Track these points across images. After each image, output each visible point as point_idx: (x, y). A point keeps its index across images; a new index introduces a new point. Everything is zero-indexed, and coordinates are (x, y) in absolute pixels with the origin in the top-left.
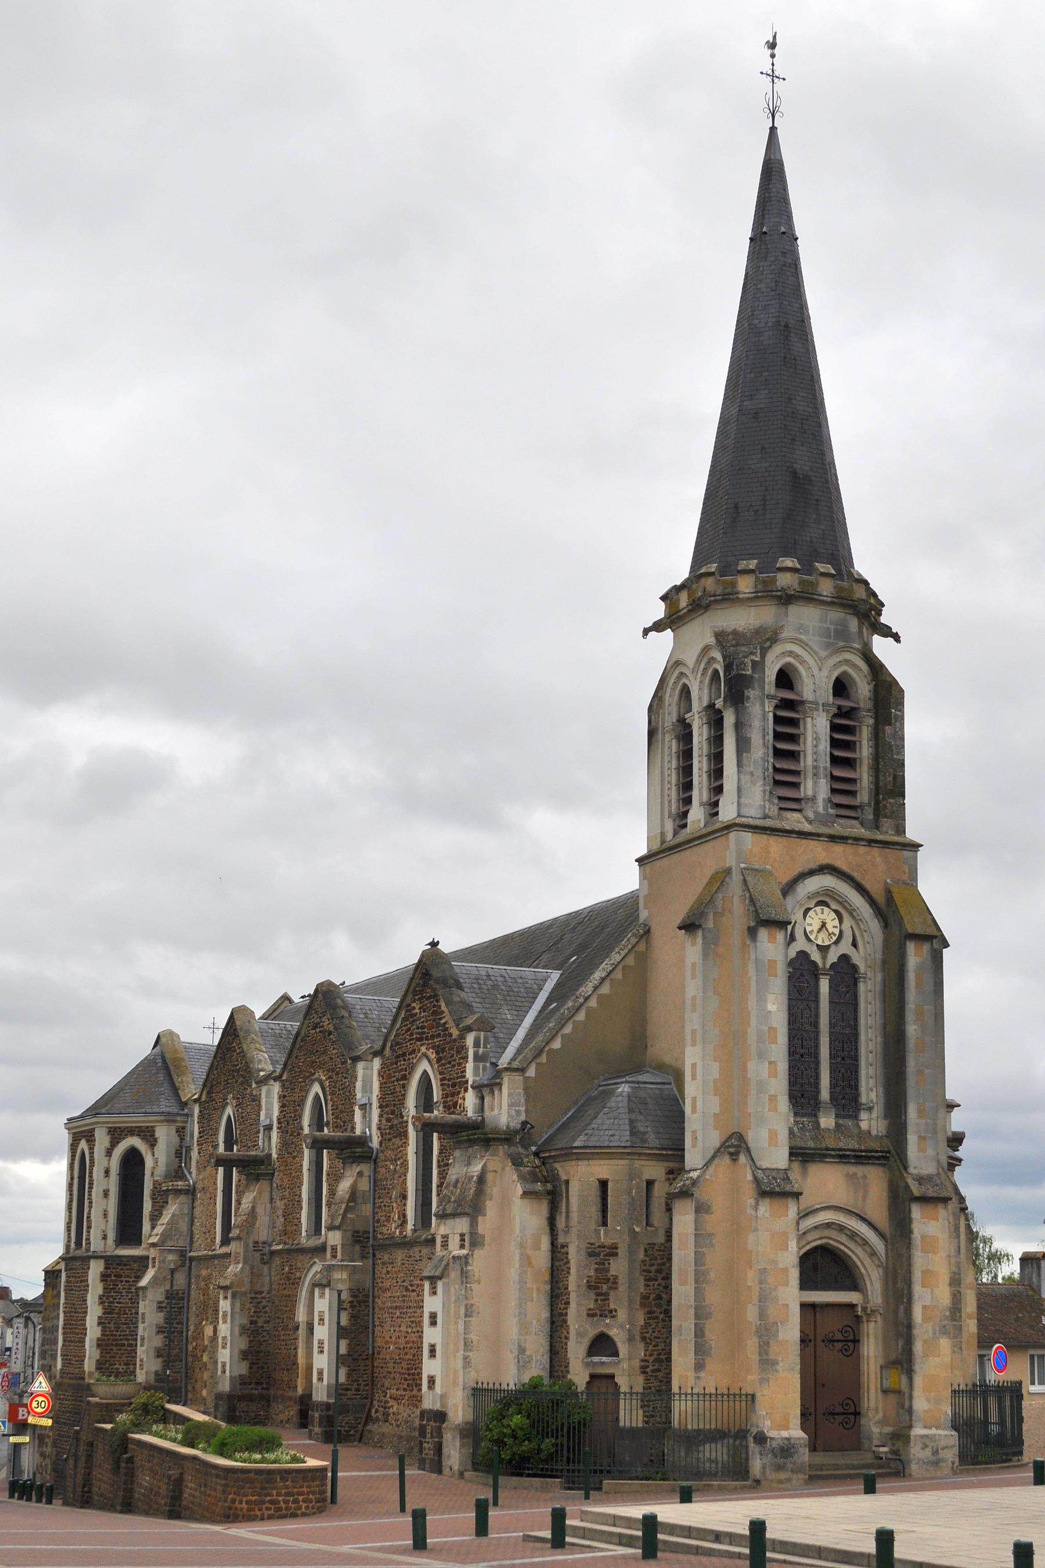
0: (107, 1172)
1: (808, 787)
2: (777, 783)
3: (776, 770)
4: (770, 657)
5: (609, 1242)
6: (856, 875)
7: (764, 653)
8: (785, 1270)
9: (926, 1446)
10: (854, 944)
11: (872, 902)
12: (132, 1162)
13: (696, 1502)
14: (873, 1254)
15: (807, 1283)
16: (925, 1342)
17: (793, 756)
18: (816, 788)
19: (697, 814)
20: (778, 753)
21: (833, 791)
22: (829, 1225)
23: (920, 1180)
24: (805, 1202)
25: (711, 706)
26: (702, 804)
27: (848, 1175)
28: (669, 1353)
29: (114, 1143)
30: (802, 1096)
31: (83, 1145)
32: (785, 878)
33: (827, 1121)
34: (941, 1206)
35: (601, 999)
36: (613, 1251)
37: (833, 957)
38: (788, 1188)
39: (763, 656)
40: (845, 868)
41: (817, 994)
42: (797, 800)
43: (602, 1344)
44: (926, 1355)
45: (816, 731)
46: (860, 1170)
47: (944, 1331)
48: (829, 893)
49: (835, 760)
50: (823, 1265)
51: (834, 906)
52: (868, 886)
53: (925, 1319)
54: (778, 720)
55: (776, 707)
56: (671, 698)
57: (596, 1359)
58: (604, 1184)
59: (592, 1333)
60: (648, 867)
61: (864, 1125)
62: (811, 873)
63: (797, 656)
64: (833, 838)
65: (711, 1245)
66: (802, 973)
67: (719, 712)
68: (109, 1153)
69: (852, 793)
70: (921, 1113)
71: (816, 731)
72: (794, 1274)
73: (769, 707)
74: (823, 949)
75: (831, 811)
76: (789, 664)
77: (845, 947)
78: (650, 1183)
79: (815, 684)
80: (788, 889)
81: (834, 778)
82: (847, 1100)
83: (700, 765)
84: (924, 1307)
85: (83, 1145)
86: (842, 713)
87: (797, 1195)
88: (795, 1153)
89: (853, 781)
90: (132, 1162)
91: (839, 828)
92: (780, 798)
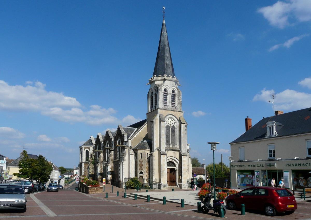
0: (84, 153)
1: (168, 104)
2: (164, 103)
3: (164, 102)
4: (163, 87)
5: (142, 160)
6: (175, 115)
7: (162, 87)
8: (165, 164)
9: (184, 185)
10: (175, 124)
11: (177, 119)
12: (87, 152)
13: (175, 191)
14: (177, 162)
15: (168, 165)
16: (184, 173)
17: (166, 100)
18: (170, 105)
19: (154, 108)
20: (164, 100)
21: (172, 105)
22: (171, 159)
23: (183, 153)
24: (167, 156)
25: (155, 94)
26: (154, 106)
27: (174, 153)
28: (182, 174)
29: (85, 149)
30: (167, 143)
31: (81, 149)
32: (165, 116)
33: (171, 146)
34: (165, 156)
35: (141, 131)
36: (142, 162)
37: (172, 126)
38: (165, 154)
39: (162, 87)
40: (173, 114)
41: (170, 130)
42: (167, 106)
43: (141, 173)
44: (184, 174)
45: (169, 97)
46: (175, 152)
47: (186, 172)
48: (171, 118)
49: (172, 101)
50: (170, 163)
51: (172, 119)
52: (177, 117)
53: (184, 170)
54: (164, 95)
55: (164, 94)
56: (150, 93)
57: (140, 175)
58: (141, 153)
59: (140, 172)
60: (148, 115)
61: (176, 147)
62: (169, 115)
63: (167, 87)
64: (172, 111)
65: (155, 161)
66: (168, 128)
67: (156, 94)
68: (84, 150)
69: (175, 105)
70: (183, 145)
71: (169, 97)
72: (166, 164)
73: (163, 94)
74: (170, 125)
75: (172, 107)
76: (166, 88)
77: (173, 124)
78: (147, 153)
79: (170, 91)
80: (166, 117)
81: (172, 103)
82: (174, 143)
83: (154, 101)
84: (184, 169)
85: (81, 149)
86: (173, 95)
87: (166, 155)
88: (166, 150)
89: (175, 104)
90: (87, 152)
91: (172, 109)
92: (164, 105)
